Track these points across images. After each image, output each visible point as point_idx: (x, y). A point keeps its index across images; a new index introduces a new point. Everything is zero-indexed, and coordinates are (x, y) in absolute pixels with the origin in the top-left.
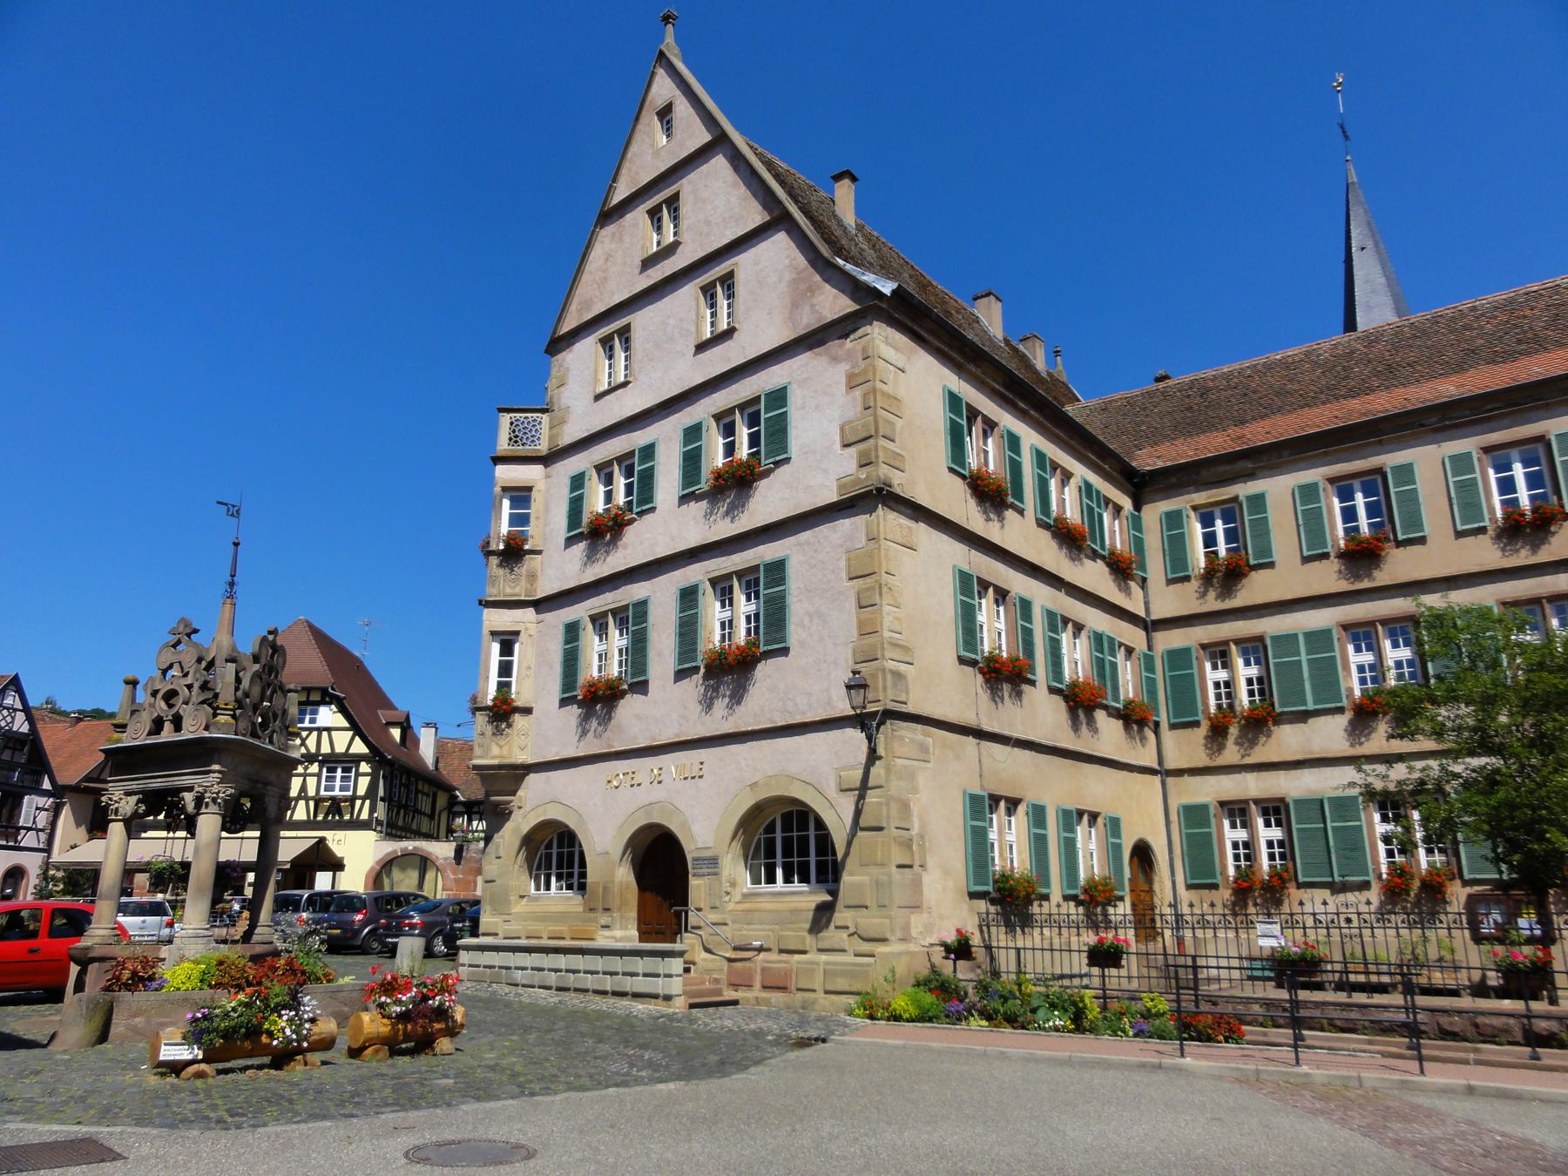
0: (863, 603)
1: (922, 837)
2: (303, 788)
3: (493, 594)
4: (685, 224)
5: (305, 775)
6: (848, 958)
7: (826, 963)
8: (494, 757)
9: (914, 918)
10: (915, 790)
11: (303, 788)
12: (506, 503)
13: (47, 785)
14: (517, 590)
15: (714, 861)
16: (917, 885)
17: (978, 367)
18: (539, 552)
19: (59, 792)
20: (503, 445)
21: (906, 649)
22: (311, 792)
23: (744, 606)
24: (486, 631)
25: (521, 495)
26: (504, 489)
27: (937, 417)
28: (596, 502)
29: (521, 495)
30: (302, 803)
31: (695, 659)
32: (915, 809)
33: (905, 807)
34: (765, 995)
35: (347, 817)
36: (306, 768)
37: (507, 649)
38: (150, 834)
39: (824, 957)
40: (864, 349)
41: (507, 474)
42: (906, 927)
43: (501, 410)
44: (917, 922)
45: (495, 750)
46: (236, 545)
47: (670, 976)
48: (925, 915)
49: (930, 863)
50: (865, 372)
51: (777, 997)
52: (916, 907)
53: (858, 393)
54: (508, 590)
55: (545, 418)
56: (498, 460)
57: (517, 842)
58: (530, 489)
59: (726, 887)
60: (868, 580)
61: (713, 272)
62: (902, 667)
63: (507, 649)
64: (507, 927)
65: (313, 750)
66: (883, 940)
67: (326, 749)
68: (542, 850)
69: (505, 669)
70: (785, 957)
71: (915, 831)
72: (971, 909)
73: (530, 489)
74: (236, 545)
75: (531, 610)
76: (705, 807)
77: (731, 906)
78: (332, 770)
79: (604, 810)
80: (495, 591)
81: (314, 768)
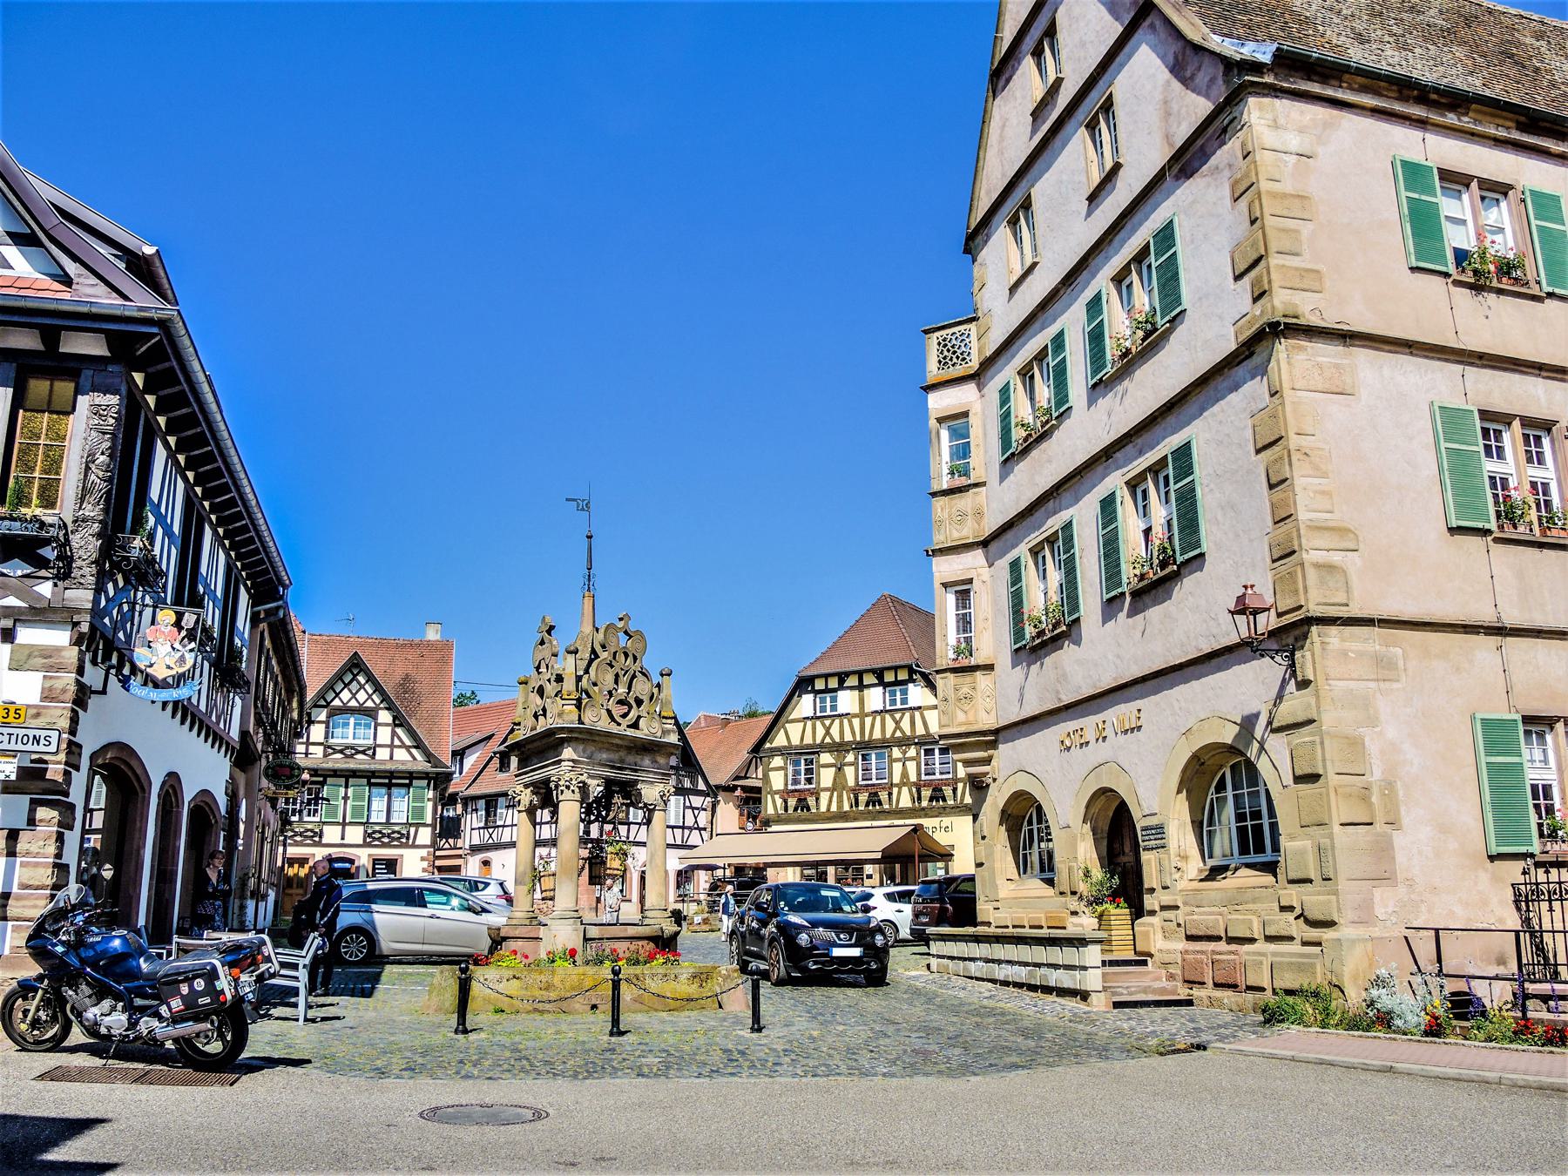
0: (1273, 481)
1: (1389, 786)
2: (905, 774)
3: (940, 539)
4: (1063, 55)
5: (904, 760)
6: (1295, 947)
7: (1274, 954)
8: (960, 725)
9: (1379, 894)
10: (1373, 721)
11: (905, 774)
12: (945, 434)
13: (701, 786)
14: (965, 532)
15: (1159, 830)
16: (1384, 850)
17: (1460, 115)
18: (983, 484)
19: (713, 791)
20: (933, 371)
21: (1342, 531)
22: (913, 778)
23: (1160, 513)
24: (937, 585)
25: (957, 420)
26: (940, 420)
27: (1386, 204)
28: (1022, 409)
29: (957, 420)
30: (905, 790)
31: (1120, 584)
32: (1373, 747)
33: (1355, 745)
34: (1219, 993)
35: (951, 802)
36: (904, 753)
37: (964, 596)
38: (774, 828)
39: (1272, 947)
40: (1243, 145)
41: (940, 402)
42: (1367, 906)
43: (926, 332)
44: (1385, 902)
45: (961, 717)
46: (590, 537)
47: (1085, 968)
48: (1402, 890)
49: (1406, 819)
50: (1247, 175)
51: (1226, 996)
52: (1386, 878)
53: (1243, 203)
54: (956, 535)
55: (973, 326)
56: (929, 388)
57: (997, 819)
58: (965, 414)
59: (1175, 861)
60: (1275, 448)
61: (1089, 106)
62: (1336, 558)
63: (964, 596)
64: (998, 914)
65: (908, 733)
66: (1330, 924)
67: (920, 730)
68: (1025, 828)
69: (965, 623)
70: (1234, 947)
71: (1376, 774)
72: (1496, 879)
73: (965, 414)
74: (590, 537)
75: (979, 552)
76: (1147, 759)
77: (1182, 885)
78: (929, 752)
79: (1057, 772)
80: (942, 538)
81: (912, 752)
